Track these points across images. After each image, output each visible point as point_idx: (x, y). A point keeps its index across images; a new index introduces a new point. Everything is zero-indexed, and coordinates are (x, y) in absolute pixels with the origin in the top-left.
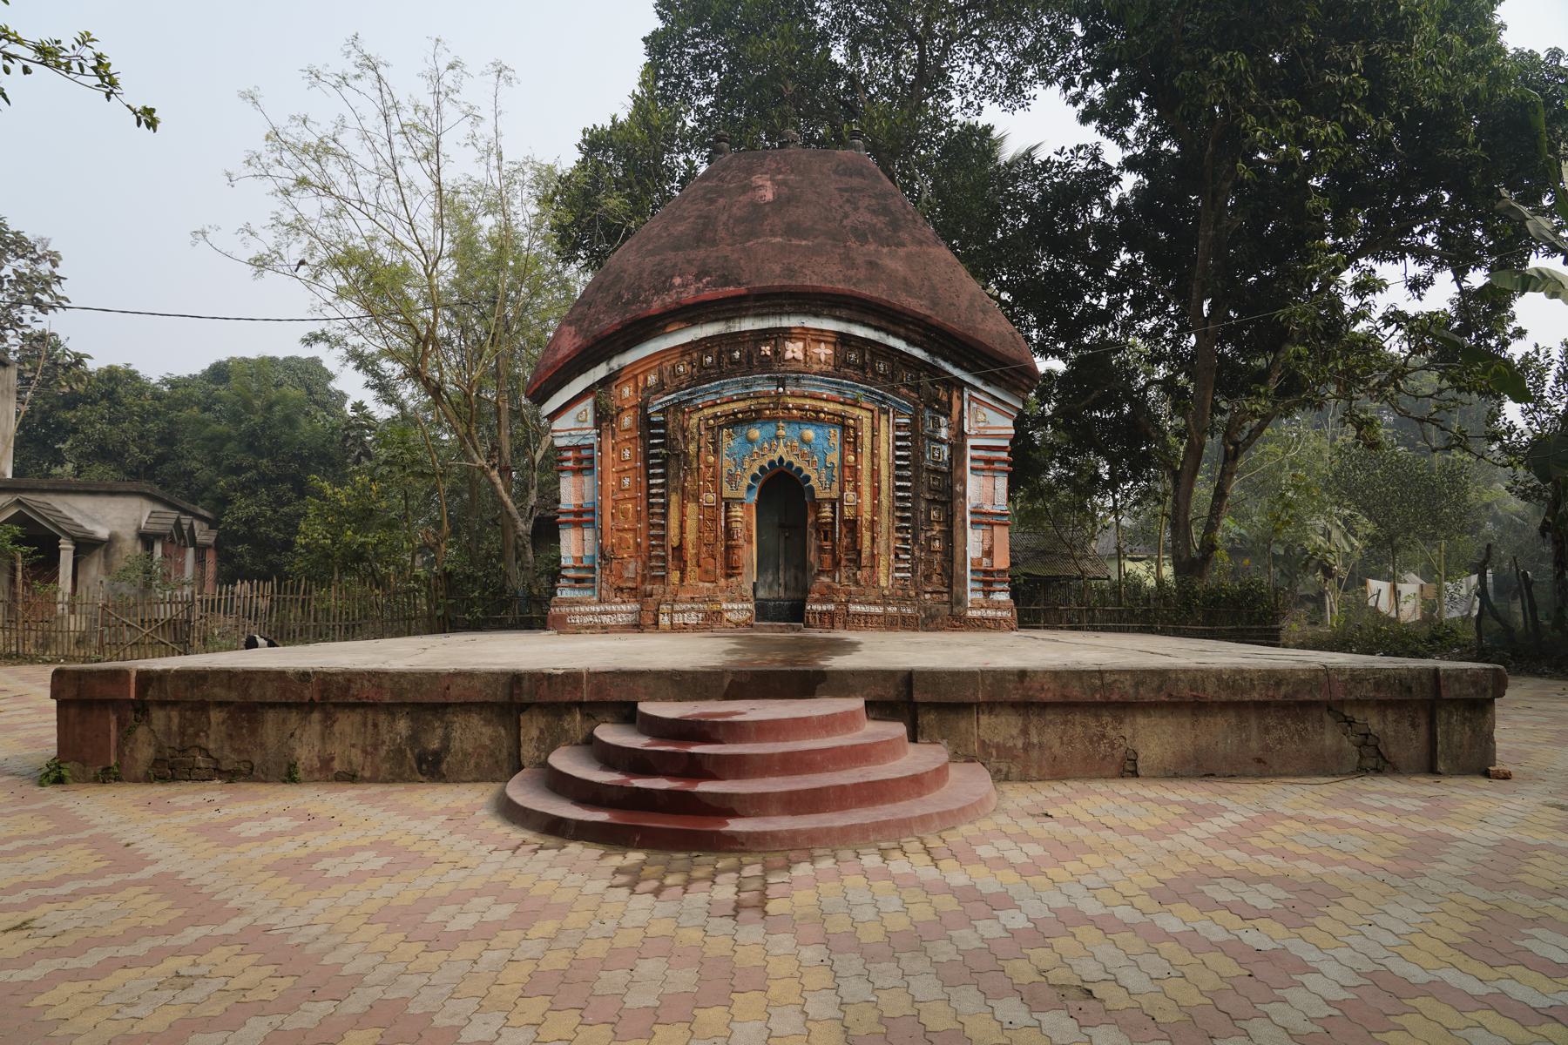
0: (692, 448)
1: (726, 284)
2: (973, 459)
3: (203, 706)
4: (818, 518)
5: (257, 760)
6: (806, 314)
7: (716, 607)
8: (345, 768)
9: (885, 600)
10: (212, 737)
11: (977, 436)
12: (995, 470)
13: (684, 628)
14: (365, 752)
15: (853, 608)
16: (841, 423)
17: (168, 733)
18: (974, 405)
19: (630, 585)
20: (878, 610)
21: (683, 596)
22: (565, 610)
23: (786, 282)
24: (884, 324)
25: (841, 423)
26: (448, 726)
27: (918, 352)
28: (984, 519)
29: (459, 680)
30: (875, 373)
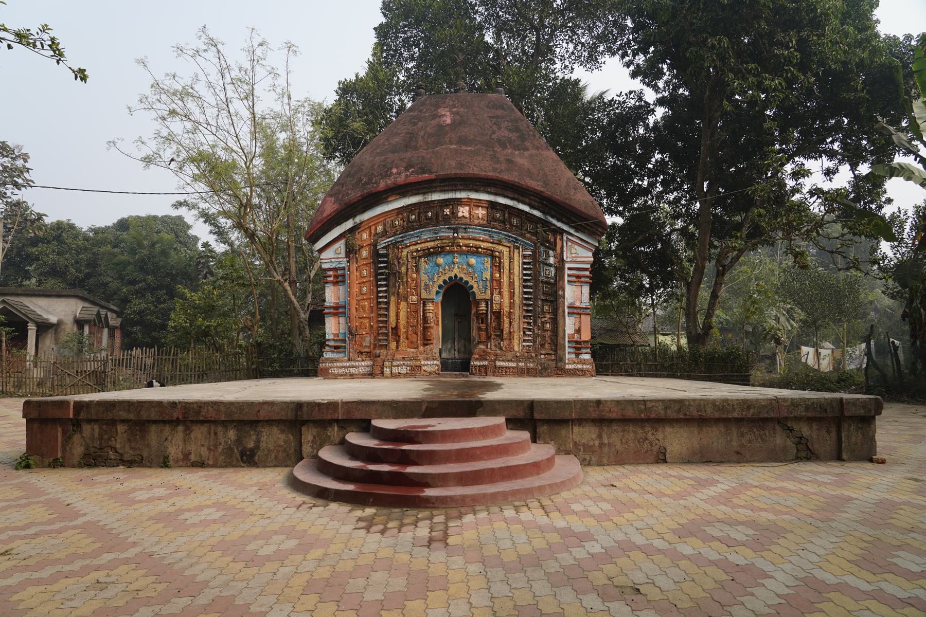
0: (403, 269)
2: (569, 275)
3: (113, 422)
5: (145, 454)
6: (470, 190)
7: (417, 363)
8: (198, 459)
9: (517, 359)
10: (119, 440)
11: (571, 262)
12: (582, 282)
13: (398, 376)
14: (209, 449)
15: (498, 363)
16: (491, 254)
17: (92, 438)
18: (569, 244)
19: (367, 350)
20: (513, 365)
21: (398, 356)
22: (328, 365)
23: (458, 171)
24: (516, 196)
25: (491, 254)
26: (259, 434)
27: (536, 213)
28: (576, 311)
29: (266, 407)
30: (512, 225)
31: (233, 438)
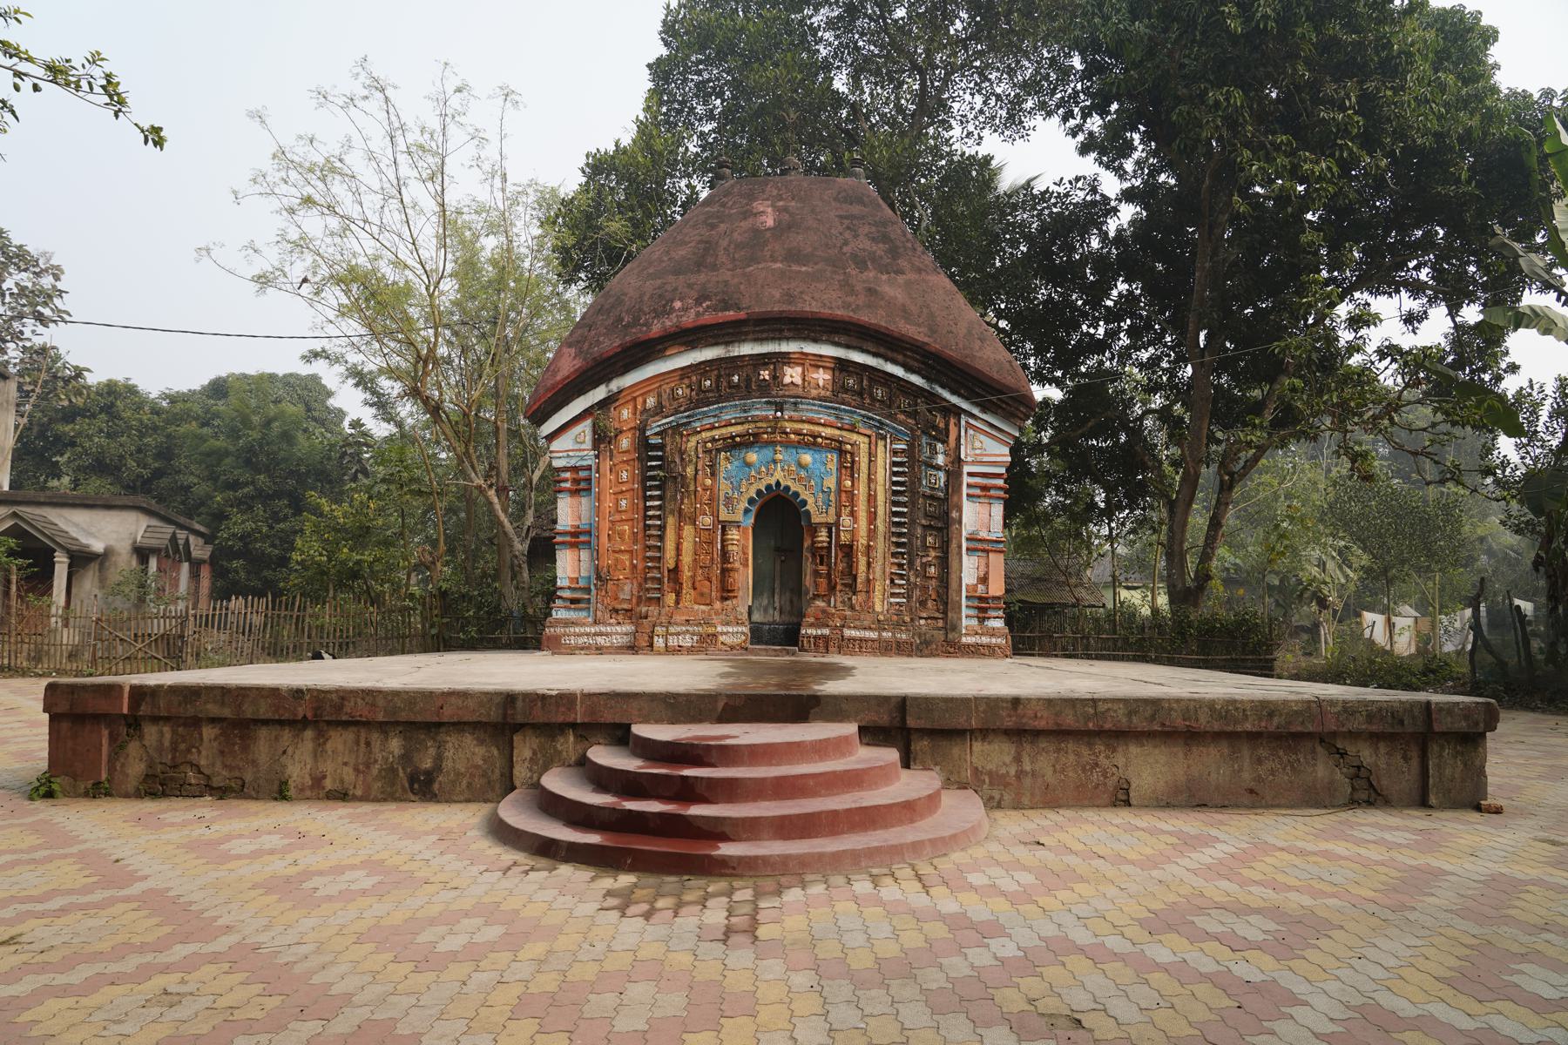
0: (690, 471)
1: (726, 309)
2: (969, 486)
3: (195, 722)
4: (814, 543)
5: (248, 777)
6: (805, 339)
7: (711, 630)
8: (337, 786)
9: (880, 626)
12: (991, 497)
13: (678, 650)
14: (356, 770)
15: (848, 633)
16: (839, 448)
18: (971, 432)
19: (625, 606)
20: (873, 635)
21: (678, 618)
22: (560, 630)
23: (785, 307)
24: (882, 350)
25: (839, 448)
26: (440, 746)
27: (916, 379)
28: (980, 546)
29: (453, 700)
30: (873, 399)
31: (397, 752)
